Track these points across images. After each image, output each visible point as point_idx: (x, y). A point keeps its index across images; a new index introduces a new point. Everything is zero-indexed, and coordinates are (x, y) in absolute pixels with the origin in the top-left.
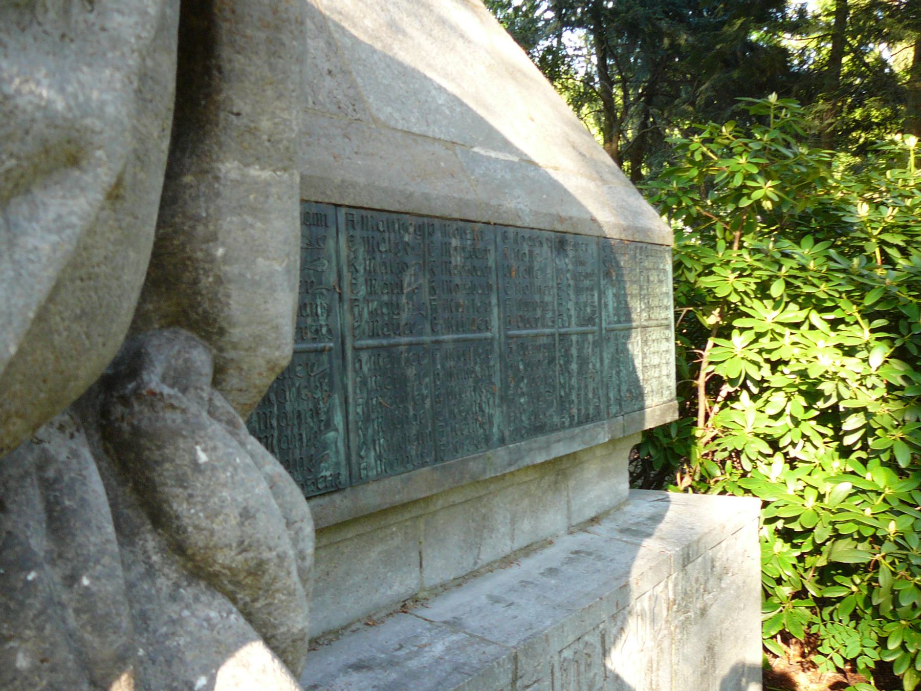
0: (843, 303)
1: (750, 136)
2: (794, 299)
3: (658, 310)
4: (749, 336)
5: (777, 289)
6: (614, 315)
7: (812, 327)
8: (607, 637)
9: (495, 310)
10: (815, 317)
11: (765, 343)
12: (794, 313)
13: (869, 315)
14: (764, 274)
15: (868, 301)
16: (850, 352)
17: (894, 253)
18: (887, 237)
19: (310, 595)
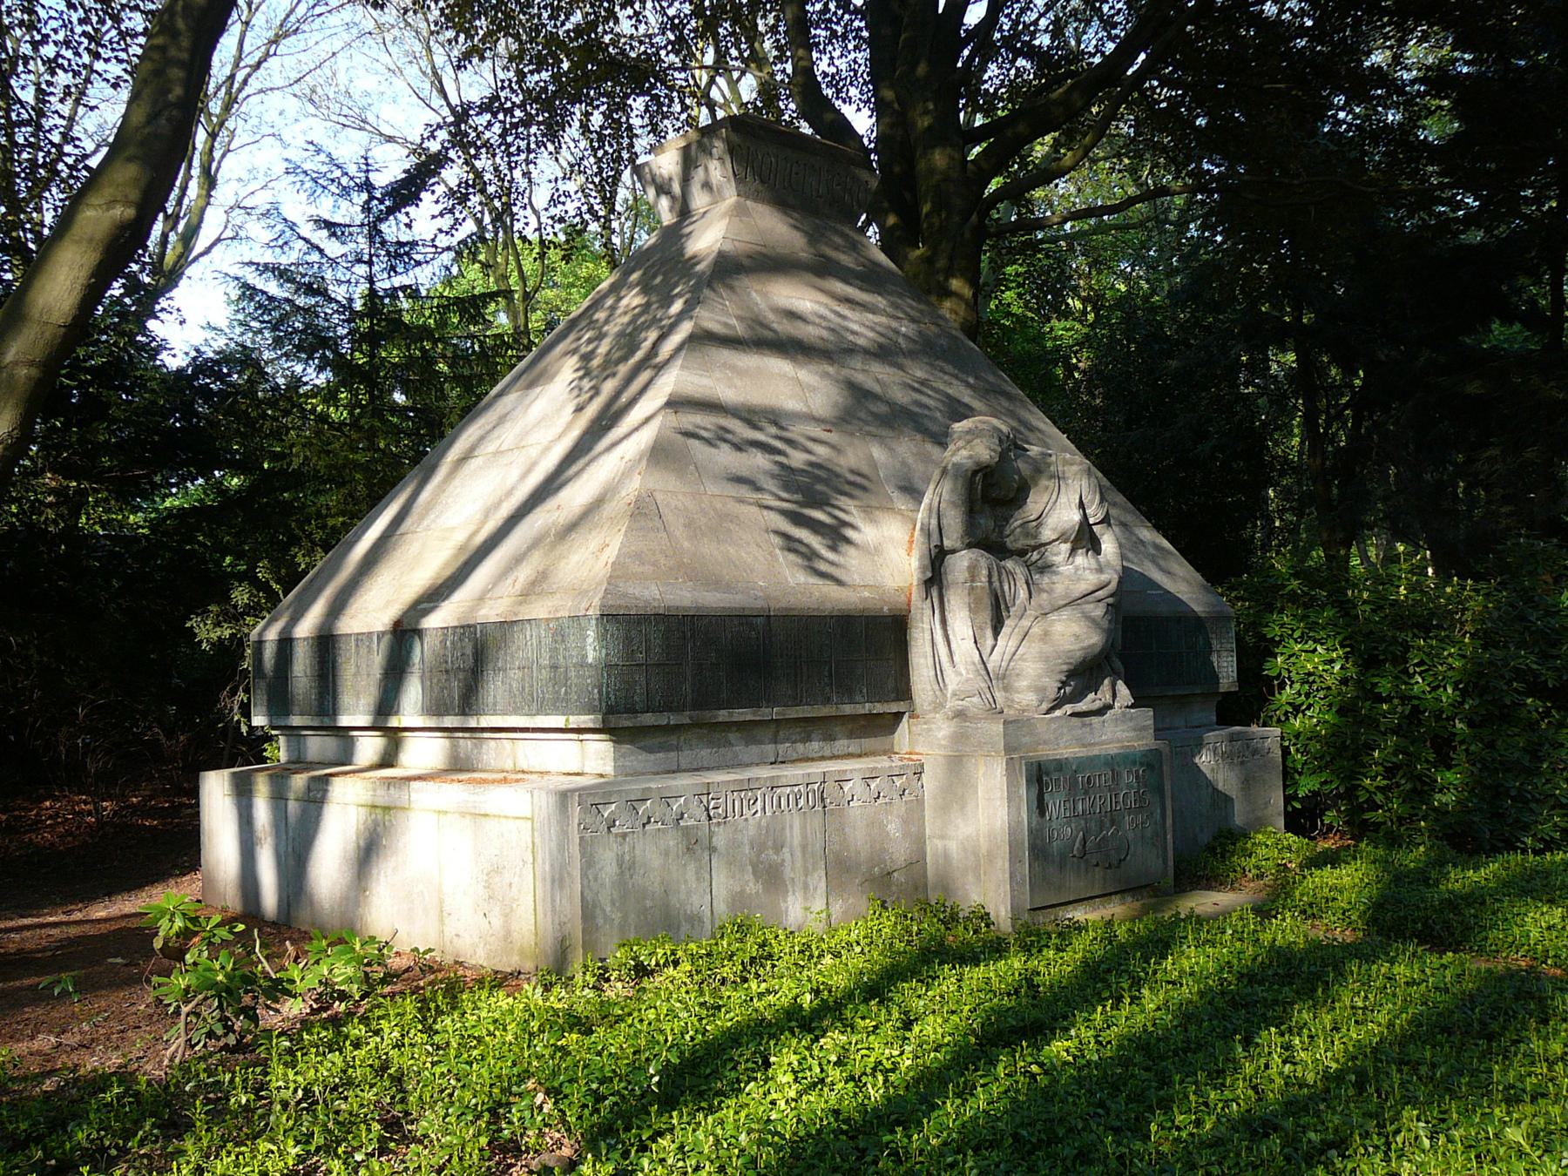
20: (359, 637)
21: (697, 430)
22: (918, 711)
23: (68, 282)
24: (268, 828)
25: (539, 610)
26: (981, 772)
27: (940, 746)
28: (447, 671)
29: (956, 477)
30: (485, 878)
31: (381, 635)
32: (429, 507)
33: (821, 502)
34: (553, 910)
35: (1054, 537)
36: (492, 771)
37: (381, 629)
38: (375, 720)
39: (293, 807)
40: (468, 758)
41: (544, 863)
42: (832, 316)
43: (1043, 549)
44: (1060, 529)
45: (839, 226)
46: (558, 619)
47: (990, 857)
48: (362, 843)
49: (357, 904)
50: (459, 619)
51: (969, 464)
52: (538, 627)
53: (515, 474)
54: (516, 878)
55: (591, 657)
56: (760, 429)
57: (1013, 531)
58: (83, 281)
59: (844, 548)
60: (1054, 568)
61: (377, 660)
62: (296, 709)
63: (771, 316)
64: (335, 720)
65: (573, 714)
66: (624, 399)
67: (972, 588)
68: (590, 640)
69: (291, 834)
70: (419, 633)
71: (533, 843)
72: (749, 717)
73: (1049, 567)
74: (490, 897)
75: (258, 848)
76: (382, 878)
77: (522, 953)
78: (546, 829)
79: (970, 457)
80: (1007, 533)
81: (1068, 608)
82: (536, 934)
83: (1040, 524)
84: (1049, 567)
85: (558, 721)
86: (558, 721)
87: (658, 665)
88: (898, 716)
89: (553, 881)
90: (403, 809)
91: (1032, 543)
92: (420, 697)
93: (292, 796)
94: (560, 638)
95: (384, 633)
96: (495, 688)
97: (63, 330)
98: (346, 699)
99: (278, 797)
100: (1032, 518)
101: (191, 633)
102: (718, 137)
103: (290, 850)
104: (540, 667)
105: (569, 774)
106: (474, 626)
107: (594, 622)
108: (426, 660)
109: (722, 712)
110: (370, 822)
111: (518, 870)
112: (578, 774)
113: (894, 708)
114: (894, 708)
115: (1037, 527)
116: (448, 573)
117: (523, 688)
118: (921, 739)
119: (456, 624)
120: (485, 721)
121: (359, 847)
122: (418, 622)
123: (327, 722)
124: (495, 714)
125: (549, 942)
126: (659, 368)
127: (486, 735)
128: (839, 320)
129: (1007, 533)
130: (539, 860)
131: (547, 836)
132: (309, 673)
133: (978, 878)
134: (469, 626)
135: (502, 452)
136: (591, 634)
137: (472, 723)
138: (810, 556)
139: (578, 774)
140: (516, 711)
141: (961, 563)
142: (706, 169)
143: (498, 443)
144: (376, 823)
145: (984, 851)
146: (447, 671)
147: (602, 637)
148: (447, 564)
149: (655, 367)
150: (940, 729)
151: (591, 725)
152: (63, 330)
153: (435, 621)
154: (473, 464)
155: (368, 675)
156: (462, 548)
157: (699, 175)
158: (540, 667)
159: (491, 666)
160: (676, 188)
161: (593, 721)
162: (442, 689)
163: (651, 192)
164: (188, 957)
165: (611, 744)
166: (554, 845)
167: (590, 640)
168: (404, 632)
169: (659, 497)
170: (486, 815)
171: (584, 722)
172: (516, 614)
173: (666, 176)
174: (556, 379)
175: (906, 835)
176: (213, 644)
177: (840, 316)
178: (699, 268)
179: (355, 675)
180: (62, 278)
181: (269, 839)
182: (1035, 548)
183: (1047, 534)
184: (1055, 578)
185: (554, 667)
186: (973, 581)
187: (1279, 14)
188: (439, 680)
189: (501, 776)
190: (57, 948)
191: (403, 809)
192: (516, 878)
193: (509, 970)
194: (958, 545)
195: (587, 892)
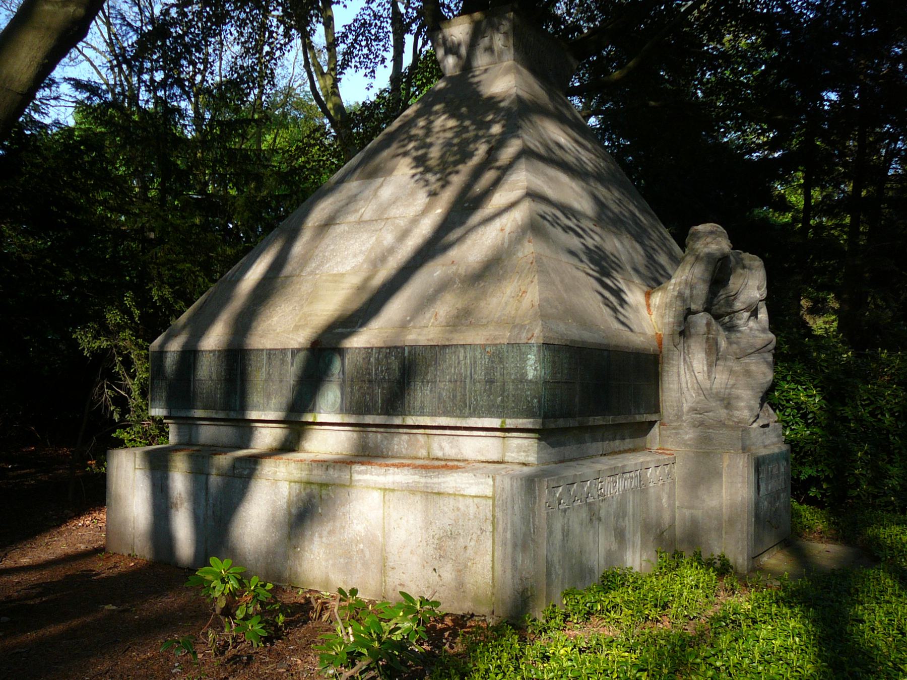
0: (808, 383)
1: (214, 588)
2: (793, 381)
3: (513, 295)
4: (780, 392)
5: (789, 378)
6: (54, 6)
7: (799, 390)
8: (611, 312)
9: (61, 627)
10: (799, 387)
11: (785, 394)
12: (793, 386)
13: (816, 387)
14: (785, 374)
15: (815, 383)
16: (810, 396)
17: (824, 368)
18: (822, 364)
19: (584, 523)
20: (271, 352)
21: (545, 215)
22: (665, 420)
23: (27, 60)
24: (184, 495)
25: (475, 337)
26: (725, 464)
27: (690, 446)
28: (370, 381)
29: (709, 263)
30: (436, 542)
31: (294, 352)
32: (305, 260)
33: (609, 275)
34: (514, 567)
35: (742, 308)
36: (404, 458)
37: (296, 346)
38: (287, 416)
39: (214, 480)
40: (377, 447)
41: (505, 530)
42: (573, 149)
43: (732, 315)
44: (748, 302)
45: (558, 92)
46: (496, 345)
47: (731, 522)
48: (294, 511)
49: (286, 557)
50: (384, 342)
51: (718, 254)
52: (474, 350)
53: (388, 238)
54: (473, 543)
55: (531, 374)
56: (569, 219)
57: (719, 302)
58: (38, 60)
59: (625, 306)
60: (735, 329)
61: (292, 371)
62: (199, 404)
63: (549, 142)
64: (243, 414)
65: (510, 418)
66: (478, 188)
67: (708, 339)
68: (531, 362)
69: (211, 501)
70: (341, 352)
71: (493, 516)
72: (601, 423)
73: (733, 327)
74: (440, 556)
75: (173, 511)
76: (316, 539)
77: (476, 600)
78: (509, 505)
79: (718, 250)
80: (715, 303)
81: (753, 355)
82: (494, 586)
83: (735, 299)
84: (733, 327)
85: (495, 423)
86: (495, 423)
87: (566, 383)
88: (652, 424)
89: (515, 546)
90: (344, 486)
91: (729, 310)
92: (339, 400)
93: (214, 471)
94: (497, 360)
95: (299, 350)
96: (421, 394)
97: (20, 97)
98: (255, 397)
99: (199, 472)
100: (732, 294)
101: (76, 343)
102: (506, 18)
103: (210, 513)
104: (474, 382)
105: (483, 462)
106: (403, 348)
107: (535, 349)
108: (675, 375)
109: (591, 419)
110: (303, 494)
111: (475, 537)
112: (498, 462)
113: (653, 418)
114: (653, 418)
115: (733, 300)
116: (355, 305)
117: (455, 397)
118: (670, 440)
119: (382, 345)
120: (410, 421)
121: (290, 513)
122: (339, 342)
123: (233, 415)
124: (422, 414)
125: (508, 590)
126: (505, 170)
127: (401, 430)
128: (577, 153)
129: (715, 303)
130: (500, 528)
131: (509, 512)
132: (214, 377)
133: (720, 536)
134: (396, 347)
135: (366, 222)
136: (532, 358)
137: (398, 421)
138: (615, 310)
139: (498, 462)
140: (446, 413)
141: (701, 320)
142: (491, 39)
143: (358, 215)
144: (311, 497)
145: (725, 517)
146: (370, 381)
147: (541, 361)
148: (348, 300)
149: (498, 168)
150: (687, 433)
151: (530, 426)
152: (20, 97)
153: (360, 341)
154: (338, 229)
155: (281, 381)
156: (361, 288)
157: (485, 42)
158: (474, 382)
159: (419, 379)
160: (463, 51)
161: (533, 423)
162: (364, 395)
163: (440, 53)
164: (238, 612)
165: (536, 441)
166: (517, 519)
167: (531, 362)
168: (322, 350)
169: (544, 260)
170: (439, 494)
171: (523, 424)
172: (448, 340)
173: (456, 42)
174: (395, 173)
175: (669, 505)
176: (92, 352)
177: (577, 150)
178: (502, 104)
179: (266, 380)
180: (24, 55)
181: (186, 504)
182: (728, 314)
183: (738, 305)
184: (738, 335)
185: (491, 382)
186: (709, 334)
187: (221, 79)
188: (360, 388)
189: (443, 463)
190: (40, 595)
191: (344, 486)
192: (473, 543)
193: (461, 613)
194: (701, 308)
195: (549, 554)
